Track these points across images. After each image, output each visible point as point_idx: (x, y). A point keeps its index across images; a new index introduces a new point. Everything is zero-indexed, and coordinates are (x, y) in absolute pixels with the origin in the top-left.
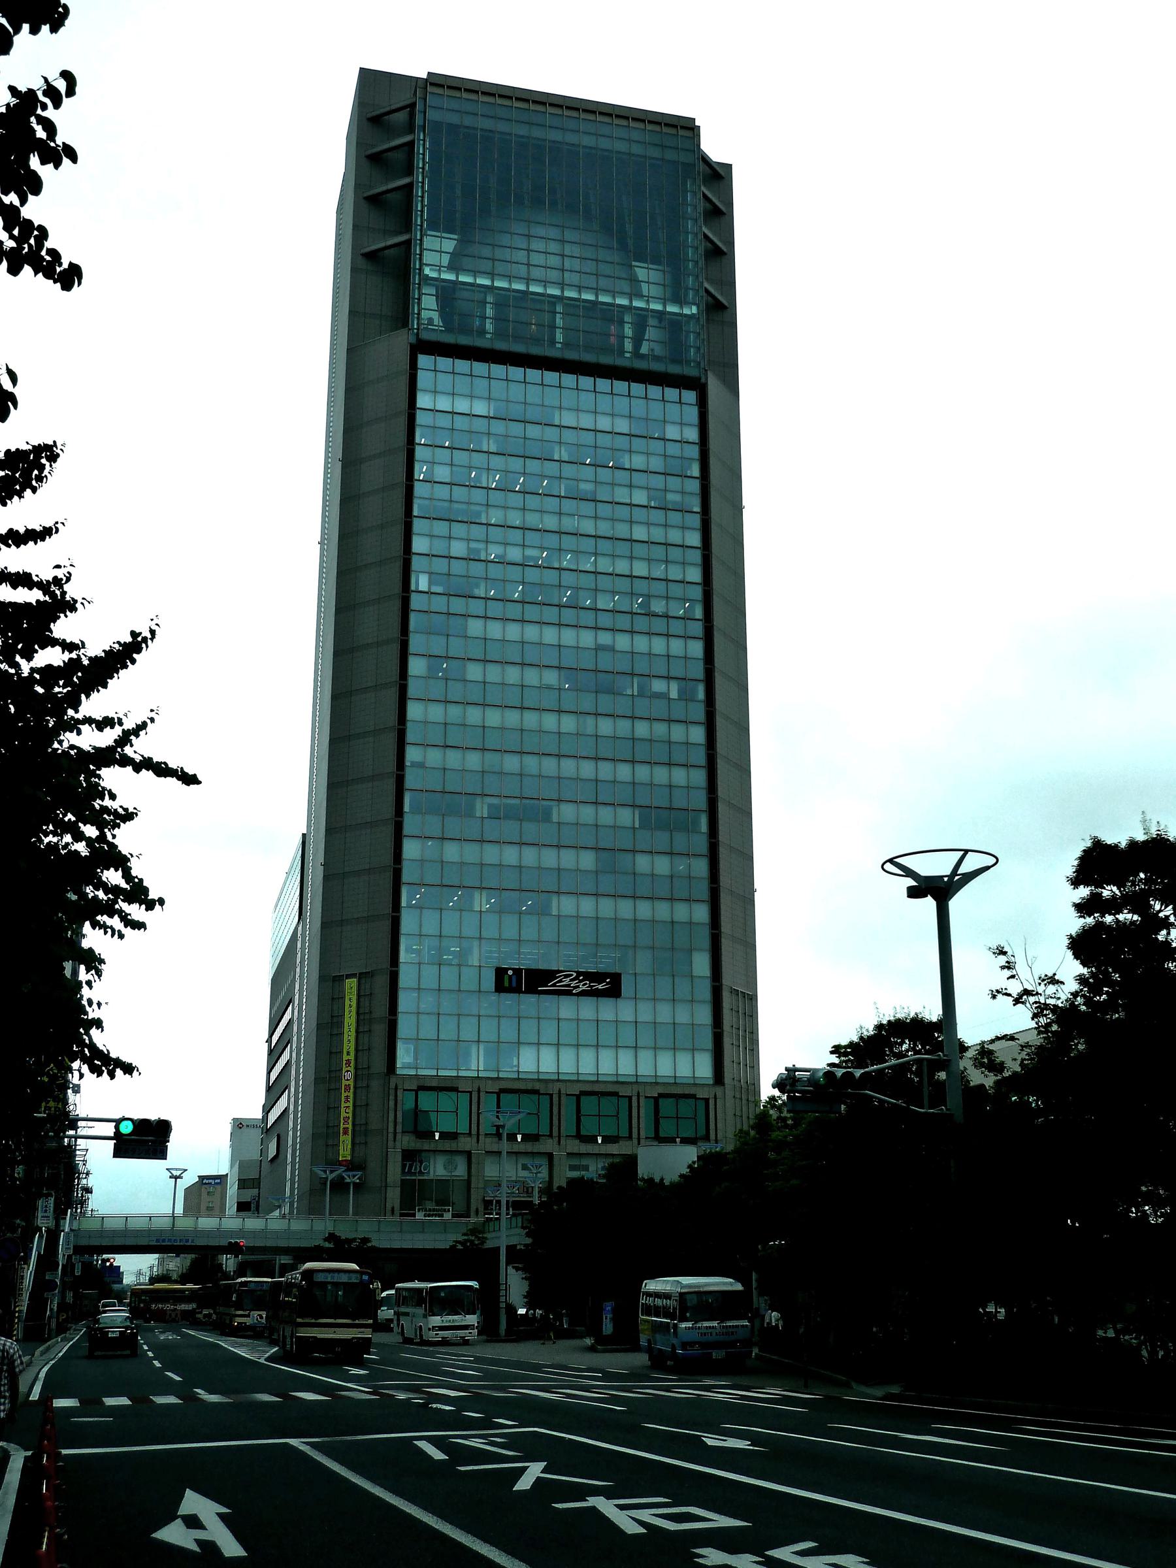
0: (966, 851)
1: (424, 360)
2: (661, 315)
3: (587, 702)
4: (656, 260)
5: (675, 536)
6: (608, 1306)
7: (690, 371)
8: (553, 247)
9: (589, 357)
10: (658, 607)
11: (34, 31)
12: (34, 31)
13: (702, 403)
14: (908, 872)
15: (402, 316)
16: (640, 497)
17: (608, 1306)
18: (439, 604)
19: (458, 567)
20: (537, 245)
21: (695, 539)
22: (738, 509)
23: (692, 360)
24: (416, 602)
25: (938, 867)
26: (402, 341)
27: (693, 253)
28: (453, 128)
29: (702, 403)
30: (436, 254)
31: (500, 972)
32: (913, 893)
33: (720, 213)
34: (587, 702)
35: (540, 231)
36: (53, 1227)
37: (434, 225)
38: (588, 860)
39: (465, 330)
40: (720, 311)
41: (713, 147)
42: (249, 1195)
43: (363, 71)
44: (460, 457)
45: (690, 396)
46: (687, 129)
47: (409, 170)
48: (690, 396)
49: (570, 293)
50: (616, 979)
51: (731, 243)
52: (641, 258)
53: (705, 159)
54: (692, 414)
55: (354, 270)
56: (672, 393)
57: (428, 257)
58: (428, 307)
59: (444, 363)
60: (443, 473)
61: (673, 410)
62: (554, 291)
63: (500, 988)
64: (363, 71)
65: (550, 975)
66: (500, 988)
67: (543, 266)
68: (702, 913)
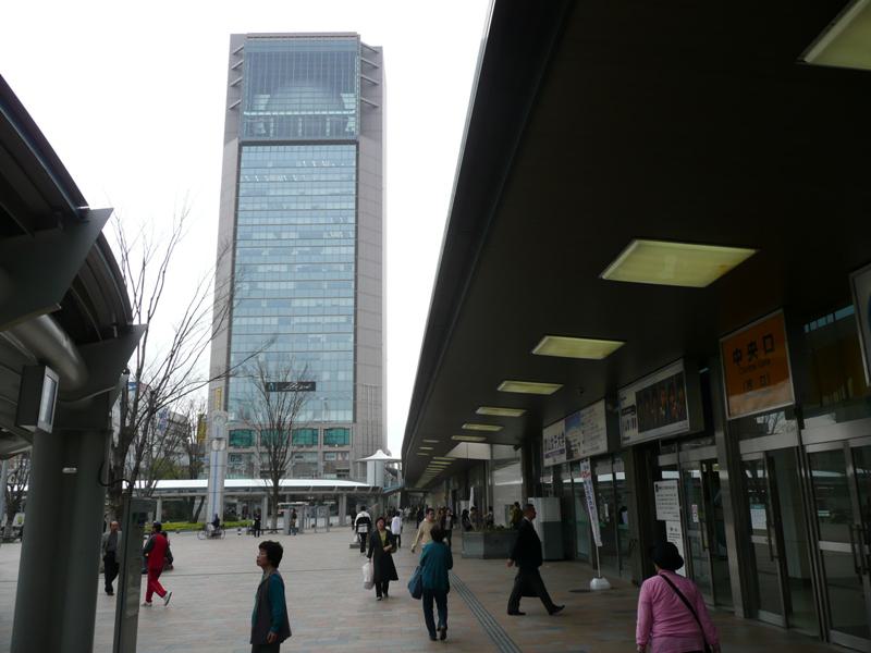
1: (245, 149)
41: (369, 40)
46: (355, 36)
50: (313, 384)
51: (381, 63)
53: (364, 46)
56: (345, 147)
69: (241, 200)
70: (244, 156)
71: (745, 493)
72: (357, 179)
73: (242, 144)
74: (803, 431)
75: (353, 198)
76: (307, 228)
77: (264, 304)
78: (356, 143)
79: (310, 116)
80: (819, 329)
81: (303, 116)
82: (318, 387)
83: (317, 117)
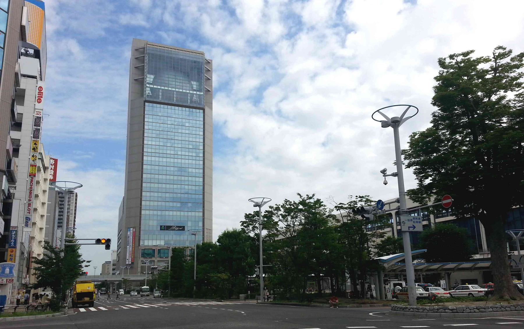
0: (410, 106)
1: (146, 103)
2: (196, 94)
3: (179, 173)
6: (426, 250)
7: (201, 106)
9: (181, 104)
11: (80, 256)
12: (80, 256)
13: (204, 113)
17: (426, 250)
20: (170, 79)
28: (153, 54)
29: (204, 113)
30: (150, 78)
31: (161, 226)
34: (179, 173)
37: (148, 73)
38: (179, 205)
42: (114, 267)
45: (202, 111)
49: (177, 90)
50: (184, 227)
56: (198, 111)
57: (147, 79)
58: (148, 91)
65: (171, 227)
66: (161, 229)
72: (204, 128)
81: (177, 91)
82: (186, 229)
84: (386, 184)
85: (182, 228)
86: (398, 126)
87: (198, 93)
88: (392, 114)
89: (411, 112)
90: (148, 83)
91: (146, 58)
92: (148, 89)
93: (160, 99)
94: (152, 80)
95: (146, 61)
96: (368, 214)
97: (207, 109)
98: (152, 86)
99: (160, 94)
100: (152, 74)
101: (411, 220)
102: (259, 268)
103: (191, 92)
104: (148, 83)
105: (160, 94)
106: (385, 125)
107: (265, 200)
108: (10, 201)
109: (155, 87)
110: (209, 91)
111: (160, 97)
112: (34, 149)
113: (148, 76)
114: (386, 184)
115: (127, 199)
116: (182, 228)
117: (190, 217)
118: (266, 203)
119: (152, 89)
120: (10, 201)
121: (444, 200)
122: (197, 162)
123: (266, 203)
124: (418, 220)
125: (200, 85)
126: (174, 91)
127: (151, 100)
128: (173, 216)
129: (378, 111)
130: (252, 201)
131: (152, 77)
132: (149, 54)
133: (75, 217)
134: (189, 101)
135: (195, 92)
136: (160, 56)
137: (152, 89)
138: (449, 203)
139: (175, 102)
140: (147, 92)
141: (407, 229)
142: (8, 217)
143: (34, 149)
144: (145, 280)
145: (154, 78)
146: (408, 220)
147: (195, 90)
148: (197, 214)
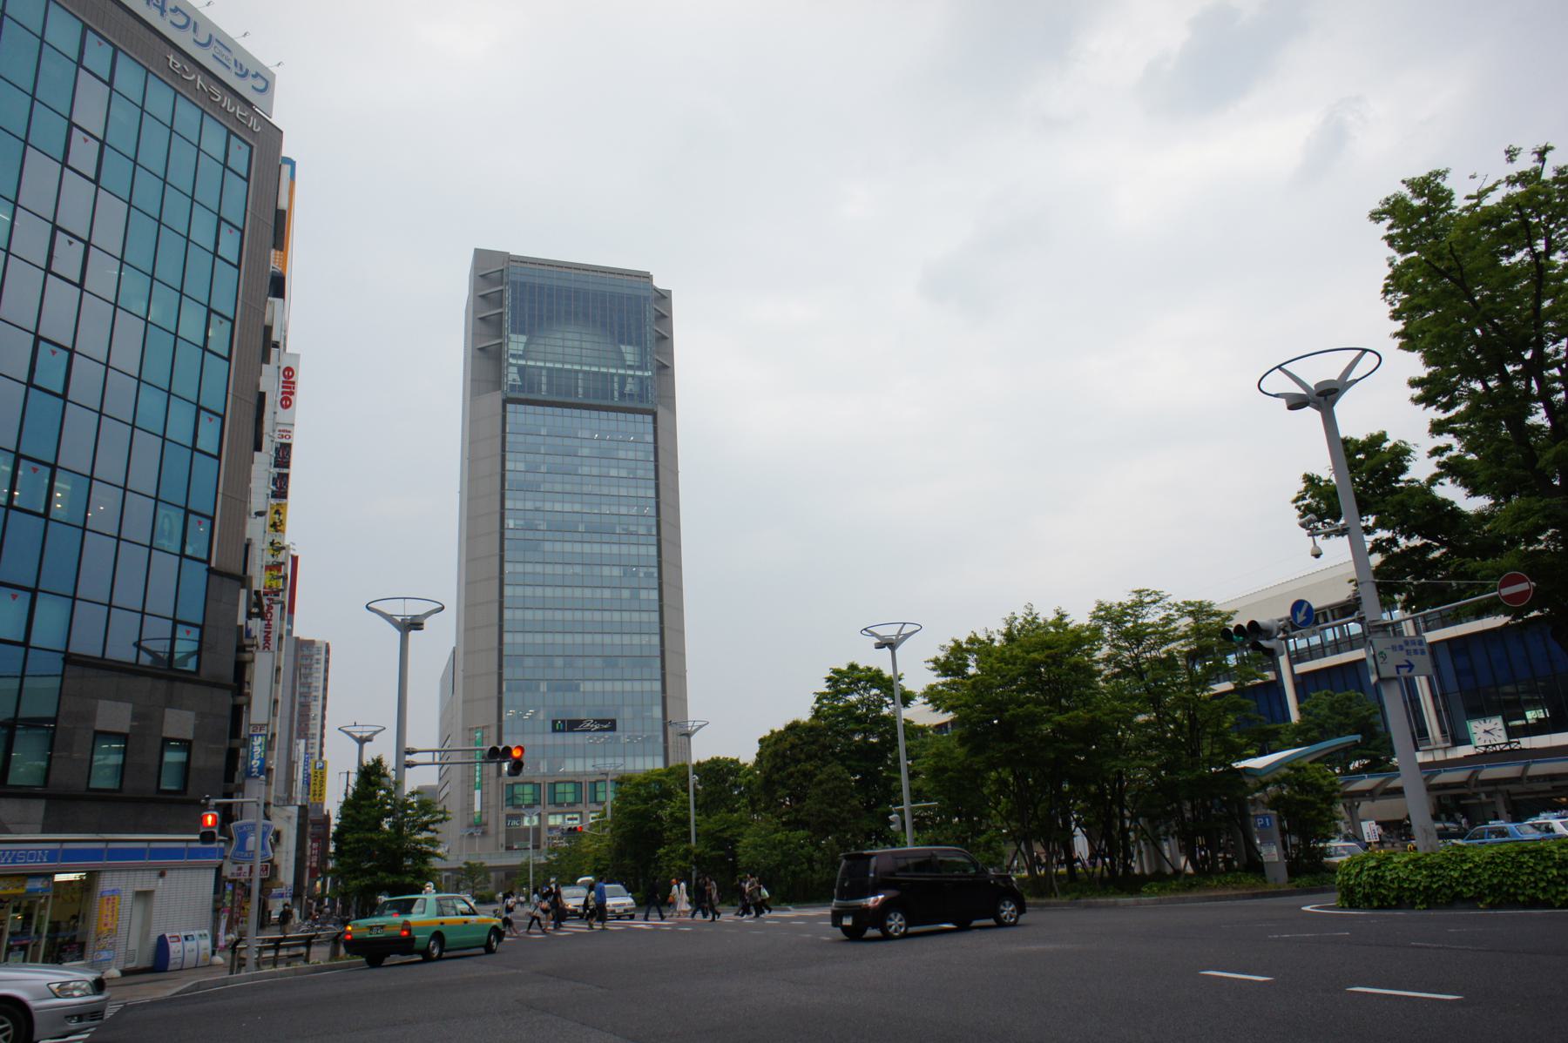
0: (1365, 351)
1: (510, 407)
2: (633, 377)
4: (630, 343)
5: (641, 493)
8: (577, 344)
10: (633, 528)
13: (655, 421)
14: (873, 634)
15: (498, 383)
16: (623, 473)
18: (520, 535)
19: (529, 515)
21: (652, 493)
22: (675, 473)
23: (648, 398)
24: (508, 534)
25: (890, 632)
26: (497, 398)
27: (650, 337)
28: (523, 284)
29: (655, 421)
30: (516, 343)
31: (554, 722)
32: (879, 646)
33: (664, 317)
35: (569, 336)
36: (416, 946)
39: (531, 391)
40: (665, 369)
41: (659, 283)
43: (476, 250)
44: (530, 457)
45: (649, 418)
46: (647, 277)
47: (501, 306)
48: (649, 418)
49: (586, 368)
50: (613, 722)
51: (671, 333)
52: (622, 342)
53: (656, 290)
54: (650, 427)
55: (473, 357)
56: (639, 417)
57: (511, 345)
58: (512, 376)
59: (521, 408)
60: (521, 466)
61: (640, 427)
62: (577, 367)
63: (554, 730)
64: (476, 250)
65: (580, 722)
66: (554, 730)
67: (570, 351)
68: (657, 686)
69: (508, 494)
70: (509, 417)
71: (1428, 215)
72: (656, 460)
73: (505, 402)
74: (1283, 402)
75: (653, 484)
76: (596, 519)
77: (581, 528)
78: (655, 415)
79: (595, 373)
80: (875, 894)
81: (585, 372)
82: (619, 724)
83: (605, 375)
84: (1317, 556)
85: (610, 725)
86: (1333, 403)
87: (639, 373)
88: (1317, 373)
89: (1369, 361)
90: (513, 356)
91: (508, 295)
92: (513, 370)
93: (544, 394)
94: (521, 347)
95: (508, 302)
96: (1268, 639)
97: (661, 412)
98: (522, 362)
99: (544, 379)
100: (522, 332)
101: (1401, 648)
102: (901, 813)
103: (621, 371)
104: (513, 356)
105: (544, 379)
106: (1296, 403)
107: (907, 630)
108: (247, 656)
109: (531, 363)
110: (665, 367)
111: (544, 387)
112: (274, 525)
113: (513, 337)
114: (1317, 556)
115: (466, 653)
116: (610, 725)
117: (626, 692)
118: (907, 636)
119: (522, 369)
120: (247, 656)
121: (1503, 585)
122: (643, 550)
123: (907, 636)
124: (1412, 648)
125: (643, 354)
126: (577, 372)
127: (522, 396)
128: (593, 695)
129: (1279, 367)
130: (873, 634)
131: (523, 338)
132: (514, 283)
133: (324, 708)
134: (616, 394)
135: (630, 372)
136: (541, 287)
137: (522, 369)
138: (1524, 594)
139: (580, 398)
140: (511, 377)
141: (1393, 673)
142: (242, 699)
143: (274, 525)
144: (527, 865)
145: (527, 344)
146: (1394, 648)
147: (630, 367)
148: (647, 686)
